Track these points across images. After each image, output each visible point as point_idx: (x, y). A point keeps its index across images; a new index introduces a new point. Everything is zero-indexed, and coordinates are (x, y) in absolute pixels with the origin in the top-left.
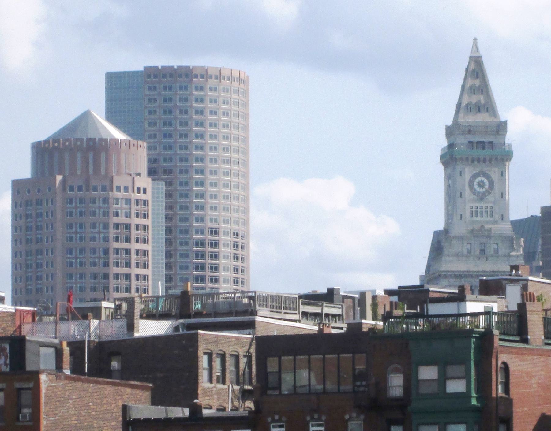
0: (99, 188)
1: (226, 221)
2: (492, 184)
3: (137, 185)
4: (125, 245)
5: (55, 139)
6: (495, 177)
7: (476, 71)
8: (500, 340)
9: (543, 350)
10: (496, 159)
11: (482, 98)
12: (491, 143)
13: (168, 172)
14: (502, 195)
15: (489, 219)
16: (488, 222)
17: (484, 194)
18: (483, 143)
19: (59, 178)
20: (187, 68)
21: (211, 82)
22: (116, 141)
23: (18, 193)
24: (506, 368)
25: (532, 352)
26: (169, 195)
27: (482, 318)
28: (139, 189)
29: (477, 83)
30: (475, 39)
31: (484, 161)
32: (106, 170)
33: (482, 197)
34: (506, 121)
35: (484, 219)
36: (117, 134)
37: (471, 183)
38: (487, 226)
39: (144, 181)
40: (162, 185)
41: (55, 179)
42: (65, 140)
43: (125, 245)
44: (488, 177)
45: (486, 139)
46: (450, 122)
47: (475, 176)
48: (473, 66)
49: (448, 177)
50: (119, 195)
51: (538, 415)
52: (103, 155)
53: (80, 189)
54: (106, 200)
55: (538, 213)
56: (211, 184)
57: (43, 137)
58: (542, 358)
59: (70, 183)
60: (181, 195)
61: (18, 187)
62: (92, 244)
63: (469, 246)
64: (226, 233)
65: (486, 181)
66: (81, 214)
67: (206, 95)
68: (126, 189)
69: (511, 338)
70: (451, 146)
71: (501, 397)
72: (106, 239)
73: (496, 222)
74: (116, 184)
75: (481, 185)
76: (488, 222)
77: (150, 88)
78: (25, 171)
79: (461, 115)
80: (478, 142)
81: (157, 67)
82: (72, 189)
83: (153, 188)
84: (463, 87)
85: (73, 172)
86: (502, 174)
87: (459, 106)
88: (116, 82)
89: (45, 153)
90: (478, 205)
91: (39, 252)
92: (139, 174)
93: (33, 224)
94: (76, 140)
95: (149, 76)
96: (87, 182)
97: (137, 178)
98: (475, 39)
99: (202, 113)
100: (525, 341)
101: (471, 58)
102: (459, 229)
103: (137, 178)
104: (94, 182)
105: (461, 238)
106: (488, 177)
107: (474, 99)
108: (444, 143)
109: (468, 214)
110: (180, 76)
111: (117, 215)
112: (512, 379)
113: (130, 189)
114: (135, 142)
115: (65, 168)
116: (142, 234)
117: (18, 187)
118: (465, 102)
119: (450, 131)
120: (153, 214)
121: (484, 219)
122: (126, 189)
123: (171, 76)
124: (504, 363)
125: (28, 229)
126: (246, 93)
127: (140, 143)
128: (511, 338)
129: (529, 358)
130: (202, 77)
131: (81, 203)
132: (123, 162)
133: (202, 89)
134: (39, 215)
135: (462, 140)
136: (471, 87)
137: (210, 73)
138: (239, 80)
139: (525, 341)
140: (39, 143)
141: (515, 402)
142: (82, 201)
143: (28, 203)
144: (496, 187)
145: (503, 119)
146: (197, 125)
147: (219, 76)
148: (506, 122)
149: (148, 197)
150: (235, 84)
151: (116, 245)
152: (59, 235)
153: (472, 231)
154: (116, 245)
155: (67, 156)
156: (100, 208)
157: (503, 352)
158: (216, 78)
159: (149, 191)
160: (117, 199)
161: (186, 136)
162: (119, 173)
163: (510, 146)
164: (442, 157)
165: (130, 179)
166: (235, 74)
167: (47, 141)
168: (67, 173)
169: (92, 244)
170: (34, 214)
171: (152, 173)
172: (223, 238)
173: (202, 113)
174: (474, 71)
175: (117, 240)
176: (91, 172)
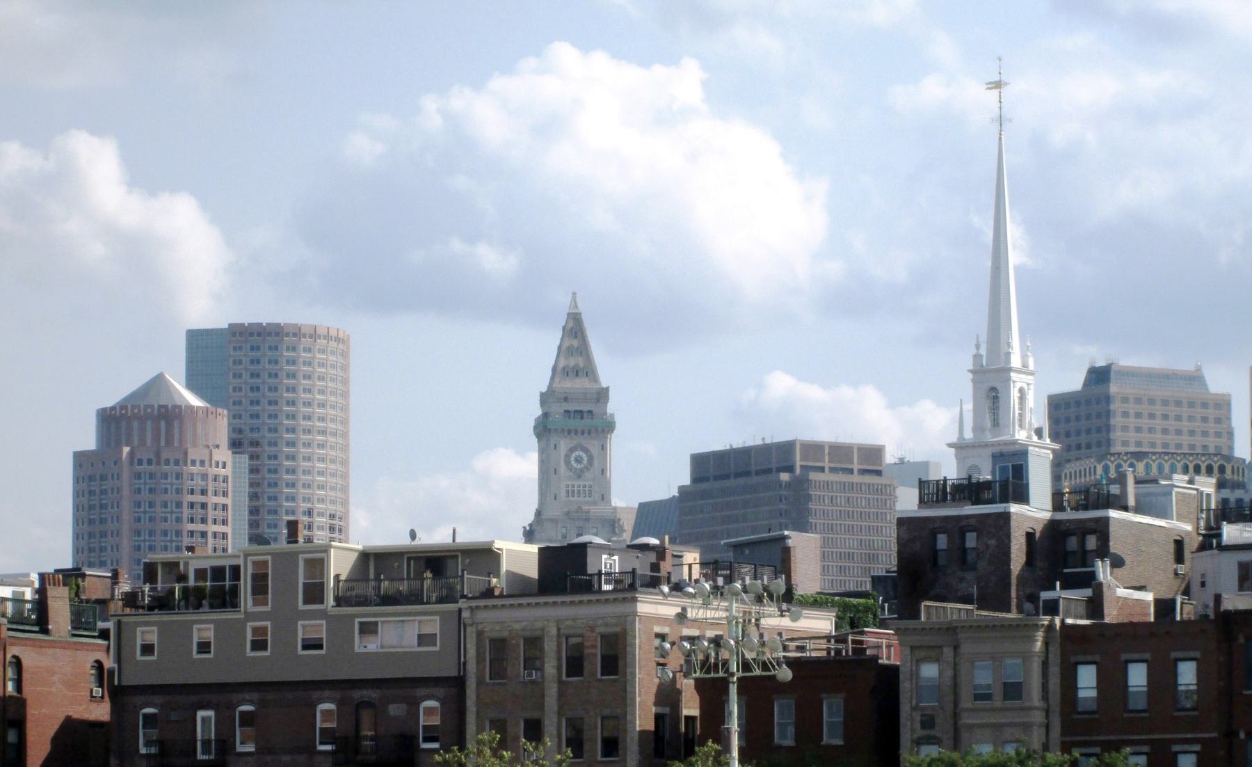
0: (172, 462)
1: (321, 501)
2: (591, 459)
3: (215, 458)
4: (201, 527)
5: (122, 405)
6: (594, 449)
7: (575, 330)
8: (9, 629)
9: (69, 643)
10: (597, 431)
11: (581, 362)
12: (590, 412)
13: (256, 444)
14: (603, 472)
15: (587, 499)
16: (587, 503)
17: (582, 470)
18: (581, 412)
19: (126, 450)
20: (278, 325)
21: (306, 342)
22: (191, 408)
23: (81, 466)
24: (18, 663)
25: (53, 644)
26: (254, 470)
27: (9, 605)
28: (217, 463)
29: (575, 343)
30: (574, 294)
31: (583, 433)
32: (181, 441)
33: (579, 475)
34: (607, 389)
35: (581, 499)
36: (194, 401)
37: (567, 456)
38: (585, 508)
39: (223, 454)
40: (245, 459)
41: (121, 451)
42: (133, 407)
43: (201, 527)
44: (586, 451)
45: (585, 408)
46: (544, 389)
47: (572, 450)
48: (571, 324)
49: (542, 451)
50: (196, 469)
51: (61, 718)
52: (176, 424)
53: (150, 462)
54: (179, 476)
55: (675, 493)
56: (304, 459)
57: (109, 404)
58: (68, 652)
59: (138, 456)
60: (270, 471)
61: (81, 459)
62: (163, 526)
63: (564, 530)
64: (321, 514)
65: (584, 455)
66: (151, 490)
67: (314, 358)
68: (202, 463)
69: (27, 628)
70: (545, 415)
71: (11, 697)
72: (179, 520)
73: (595, 503)
74: (191, 456)
75: (578, 460)
76: (587, 503)
77: (235, 349)
78: (89, 442)
79: (557, 380)
80: (576, 412)
81: (242, 325)
82: (140, 462)
83: (234, 463)
84: (560, 348)
85: (143, 441)
86: (603, 448)
87: (554, 369)
88: (199, 342)
89: (113, 422)
90: (576, 483)
91: (103, 534)
92: (218, 446)
93: (96, 502)
94: (147, 407)
95: (234, 334)
96: (158, 455)
97: (215, 451)
98: (574, 294)
99: (294, 376)
100: (45, 631)
101: (569, 314)
102: (554, 511)
103: (215, 451)
104: (164, 456)
105: (554, 521)
106: (586, 451)
107: (572, 362)
108: (539, 412)
109: (563, 494)
110: (270, 334)
111: (192, 492)
112: (26, 676)
113: (207, 463)
114: (213, 409)
115: (133, 441)
116: (220, 514)
117: (81, 459)
118: (562, 364)
119: (545, 399)
120: (233, 491)
121: (581, 499)
122: (202, 463)
123: (259, 334)
124: (14, 657)
125: (91, 507)
126: (345, 355)
127: (219, 410)
128: (27, 628)
129: (50, 651)
130: (295, 335)
131: (151, 478)
132: (199, 431)
133: (294, 349)
134: (103, 492)
135: (557, 409)
136: (568, 348)
137: (303, 331)
138: (338, 339)
139: (45, 631)
140: (104, 410)
141: (29, 702)
142: (151, 476)
143: (91, 478)
144: (596, 462)
145: (604, 385)
146: (288, 390)
147: (314, 335)
148: (607, 389)
149: (228, 471)
150: (333, 344)
151: (191, 527)
152: (126, 516)
153: (568, 513)
154: (191, 527)
155: (135, 424)
156: (172, 484)
157: (12, 644)
158: (311, 337)
159: (229, 465)
160: (192, 474)
161: (276, 403)
162: (195, 445)
163: (612, 415)
164: (535, 428)
165: (207, 451)
166: (333, 333)
167: (113, 408)
168: (136, 443)
169: (163, 526)
170: (98, 491)
171: (236, 445)
172: (318, 520)
173: (294, 376)
174: (571, 329)
175: (192, 520)
176: (163, 443)
